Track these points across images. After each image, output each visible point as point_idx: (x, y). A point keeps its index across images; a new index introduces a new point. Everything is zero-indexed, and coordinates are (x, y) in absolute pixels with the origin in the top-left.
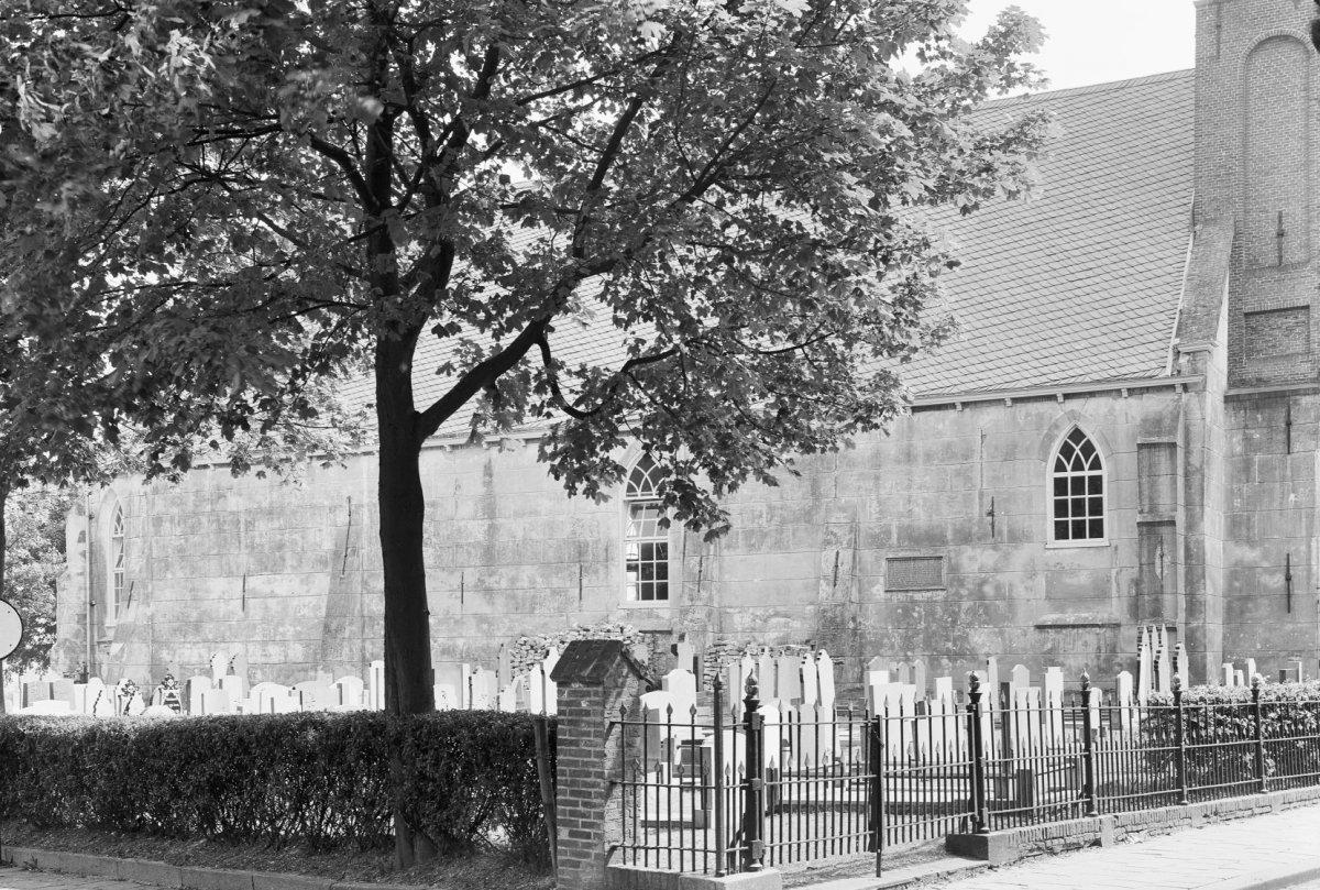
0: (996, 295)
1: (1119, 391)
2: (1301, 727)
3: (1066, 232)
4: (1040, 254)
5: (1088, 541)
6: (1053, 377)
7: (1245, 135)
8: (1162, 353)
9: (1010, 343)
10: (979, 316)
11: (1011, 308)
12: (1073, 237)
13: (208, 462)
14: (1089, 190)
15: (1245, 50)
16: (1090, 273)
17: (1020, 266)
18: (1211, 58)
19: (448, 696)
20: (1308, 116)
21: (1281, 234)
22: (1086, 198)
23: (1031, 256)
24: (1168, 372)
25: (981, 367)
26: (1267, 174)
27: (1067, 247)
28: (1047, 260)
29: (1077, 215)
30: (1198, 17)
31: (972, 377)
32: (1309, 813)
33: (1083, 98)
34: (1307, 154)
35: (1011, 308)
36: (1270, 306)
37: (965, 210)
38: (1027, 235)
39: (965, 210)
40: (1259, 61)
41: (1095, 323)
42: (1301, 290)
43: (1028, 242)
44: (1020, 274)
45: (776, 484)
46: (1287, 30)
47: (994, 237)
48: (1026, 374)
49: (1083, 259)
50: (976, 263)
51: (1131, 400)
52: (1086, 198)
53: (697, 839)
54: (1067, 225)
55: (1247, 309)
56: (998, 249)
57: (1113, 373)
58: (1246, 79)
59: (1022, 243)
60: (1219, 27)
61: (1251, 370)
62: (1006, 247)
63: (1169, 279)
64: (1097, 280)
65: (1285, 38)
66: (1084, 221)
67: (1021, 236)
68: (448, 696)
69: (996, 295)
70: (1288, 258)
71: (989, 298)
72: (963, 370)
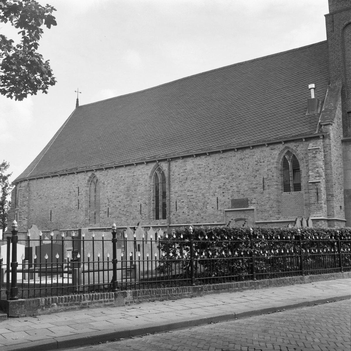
1: (302, 139)
5: (293, 193)
6: (280, 136)
9: (269, 126)
10: (260, 118)
16: (296, 103)
18: (331, 31)
19: (24, 283)
22: (297, 80)
23: (278, 99)
24: (317, 132)
29: (294, 85)
31: (256, 138)
37: (341, 207)
38: (278, 93)
39: (341, 207)
44: (275, 105)
45: (56, 10)
52: (297, 80)
53: (100, 265)
57: (300, 133)
58: (343, 37)
64: (298, 104)
66: (296, 87)
68: (24, 283)
69: (266, 112)
71: (264, 113)
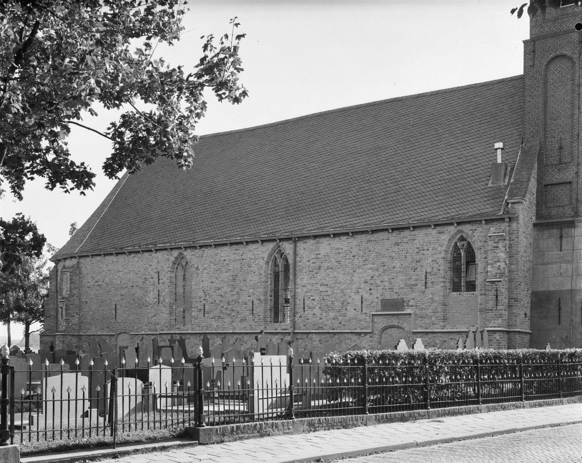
0: (434, 177)
2: (459, 377)
3: (468, 148)
4: (456, 158)
7: (545, 103)
8: (500, 203)
11: (440, 183)
12: (471, 150)
13: (101, 253)
14: (480, 129)
15: (545, 63)
16: (476, 167)
17: (446, 163)
18: (531, 66)
20: (573, 93)
21: (561, 148)
25: (423, 210)
26: (555, 120)
27: (468, 155)
28: (458, 161)
30: (525, 47)
32: (578, 406)
33: (482, 88)
34: (573, 110)
35: (440, 183)
36: (555, 181)
38: (451, 149)
40: (552, 67)
41: (475, 189)
42: (568, 175)
43: (451, 153)
46: (565, 52)
47: (437, 151)
48: (441, 213)
49: (474, 160)
50: (428, 162)
51: (201, 250)
54: (468, 145)
55: (545, 183)
56: (438, 156)
58: (546, 76)
59: (449, 153)
60: (534, 52)
61: (544, 212)
62: (441, 155)
63: (489, 170)
65: (563, 56)
66: (476, 143)
67: (448, 150)
69: (434, 177)
70: (564, 160)
71: (431, 178)
72: (415, 211)
